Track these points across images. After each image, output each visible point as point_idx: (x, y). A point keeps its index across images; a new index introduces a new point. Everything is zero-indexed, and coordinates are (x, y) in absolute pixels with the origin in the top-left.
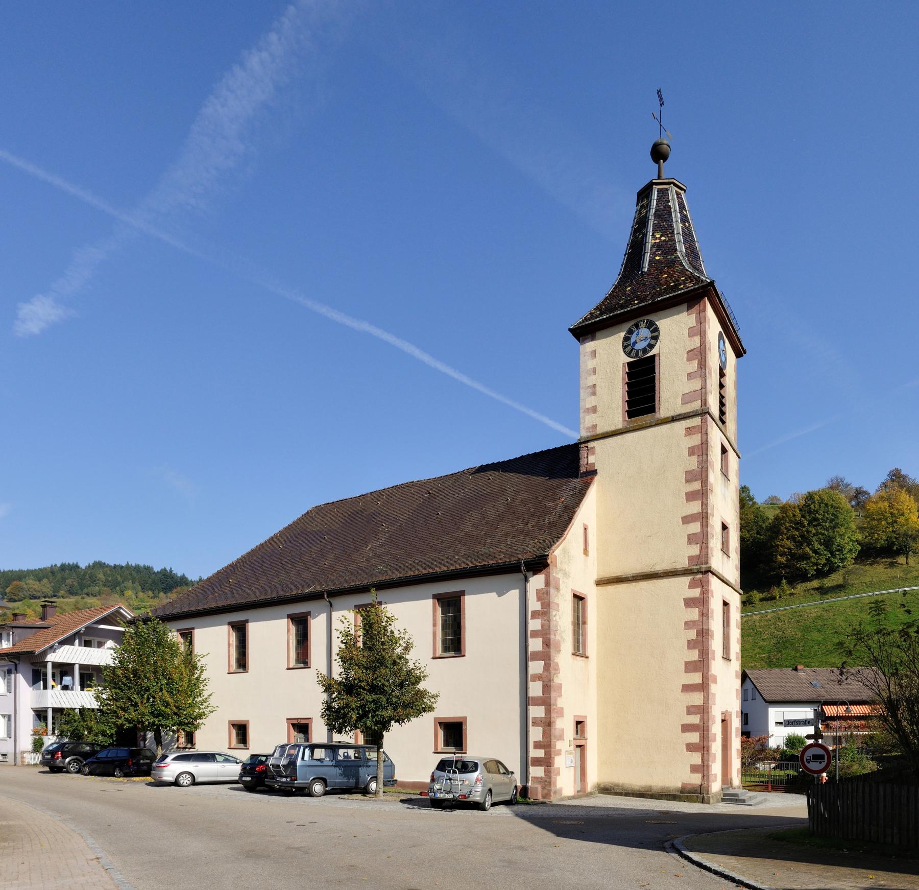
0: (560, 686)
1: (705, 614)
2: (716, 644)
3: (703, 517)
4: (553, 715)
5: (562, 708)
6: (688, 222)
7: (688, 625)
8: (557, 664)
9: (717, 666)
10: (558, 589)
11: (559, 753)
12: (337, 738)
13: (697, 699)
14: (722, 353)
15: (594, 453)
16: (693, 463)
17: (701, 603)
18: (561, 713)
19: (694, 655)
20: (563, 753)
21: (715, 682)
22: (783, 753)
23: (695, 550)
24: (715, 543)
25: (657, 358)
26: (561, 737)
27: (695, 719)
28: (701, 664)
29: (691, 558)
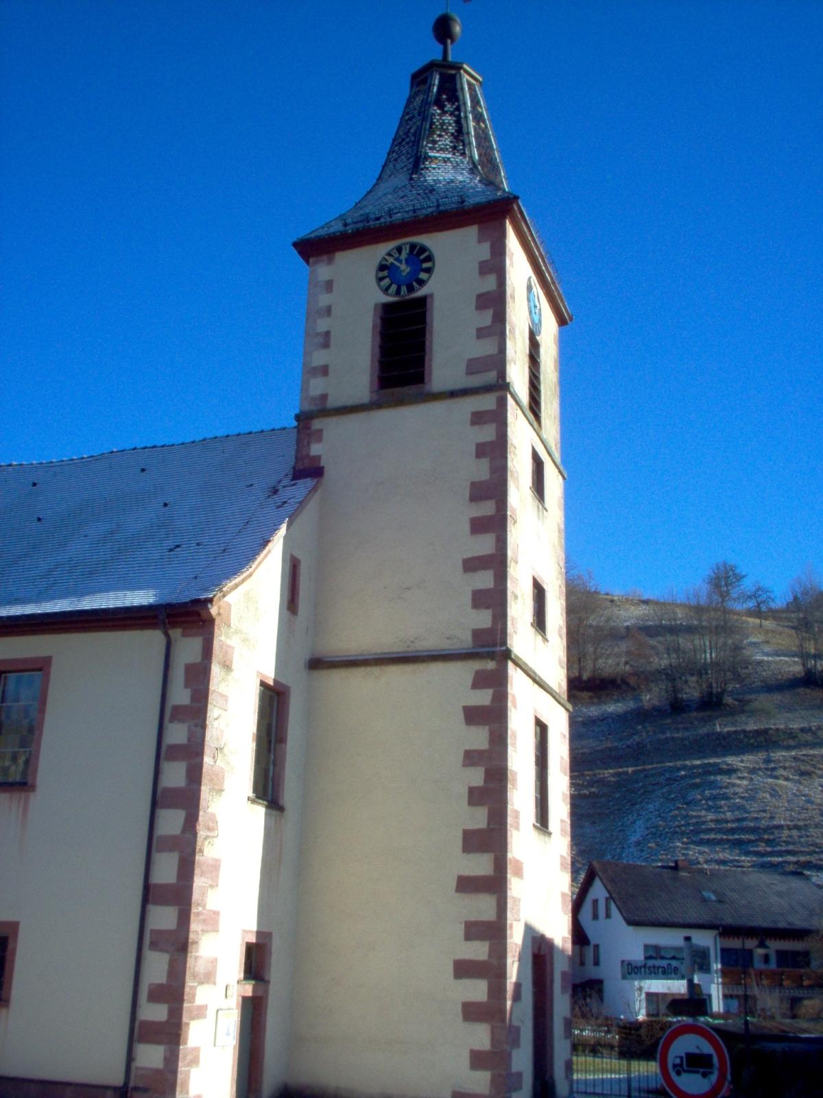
0: (215, 867)
1: (499, 739)
2: (521, 798)
3: (497, 563)
4: (194, 926)
5: (217, 913)
6: (484, 122)
7: (471, 758)
8: (213, 818)
9: (522, 840)
10: (227, 667)
11: (201, 1012)
12: (716, 982)
13: (482, 907)
14: (533, 309)
15: (320, 440)
16: (482, 470)
17: (492, 717)
18: (213, 922)
19: (479, 819)
20: (211, 1013)
21: (519, 873)
22: (492, 1052)
23: (483, 619)
24: (520, 610)
25: (429, 300)
26: (209, 978)
27: (479, 951)
28: (490, 839)
29: (477, 634)
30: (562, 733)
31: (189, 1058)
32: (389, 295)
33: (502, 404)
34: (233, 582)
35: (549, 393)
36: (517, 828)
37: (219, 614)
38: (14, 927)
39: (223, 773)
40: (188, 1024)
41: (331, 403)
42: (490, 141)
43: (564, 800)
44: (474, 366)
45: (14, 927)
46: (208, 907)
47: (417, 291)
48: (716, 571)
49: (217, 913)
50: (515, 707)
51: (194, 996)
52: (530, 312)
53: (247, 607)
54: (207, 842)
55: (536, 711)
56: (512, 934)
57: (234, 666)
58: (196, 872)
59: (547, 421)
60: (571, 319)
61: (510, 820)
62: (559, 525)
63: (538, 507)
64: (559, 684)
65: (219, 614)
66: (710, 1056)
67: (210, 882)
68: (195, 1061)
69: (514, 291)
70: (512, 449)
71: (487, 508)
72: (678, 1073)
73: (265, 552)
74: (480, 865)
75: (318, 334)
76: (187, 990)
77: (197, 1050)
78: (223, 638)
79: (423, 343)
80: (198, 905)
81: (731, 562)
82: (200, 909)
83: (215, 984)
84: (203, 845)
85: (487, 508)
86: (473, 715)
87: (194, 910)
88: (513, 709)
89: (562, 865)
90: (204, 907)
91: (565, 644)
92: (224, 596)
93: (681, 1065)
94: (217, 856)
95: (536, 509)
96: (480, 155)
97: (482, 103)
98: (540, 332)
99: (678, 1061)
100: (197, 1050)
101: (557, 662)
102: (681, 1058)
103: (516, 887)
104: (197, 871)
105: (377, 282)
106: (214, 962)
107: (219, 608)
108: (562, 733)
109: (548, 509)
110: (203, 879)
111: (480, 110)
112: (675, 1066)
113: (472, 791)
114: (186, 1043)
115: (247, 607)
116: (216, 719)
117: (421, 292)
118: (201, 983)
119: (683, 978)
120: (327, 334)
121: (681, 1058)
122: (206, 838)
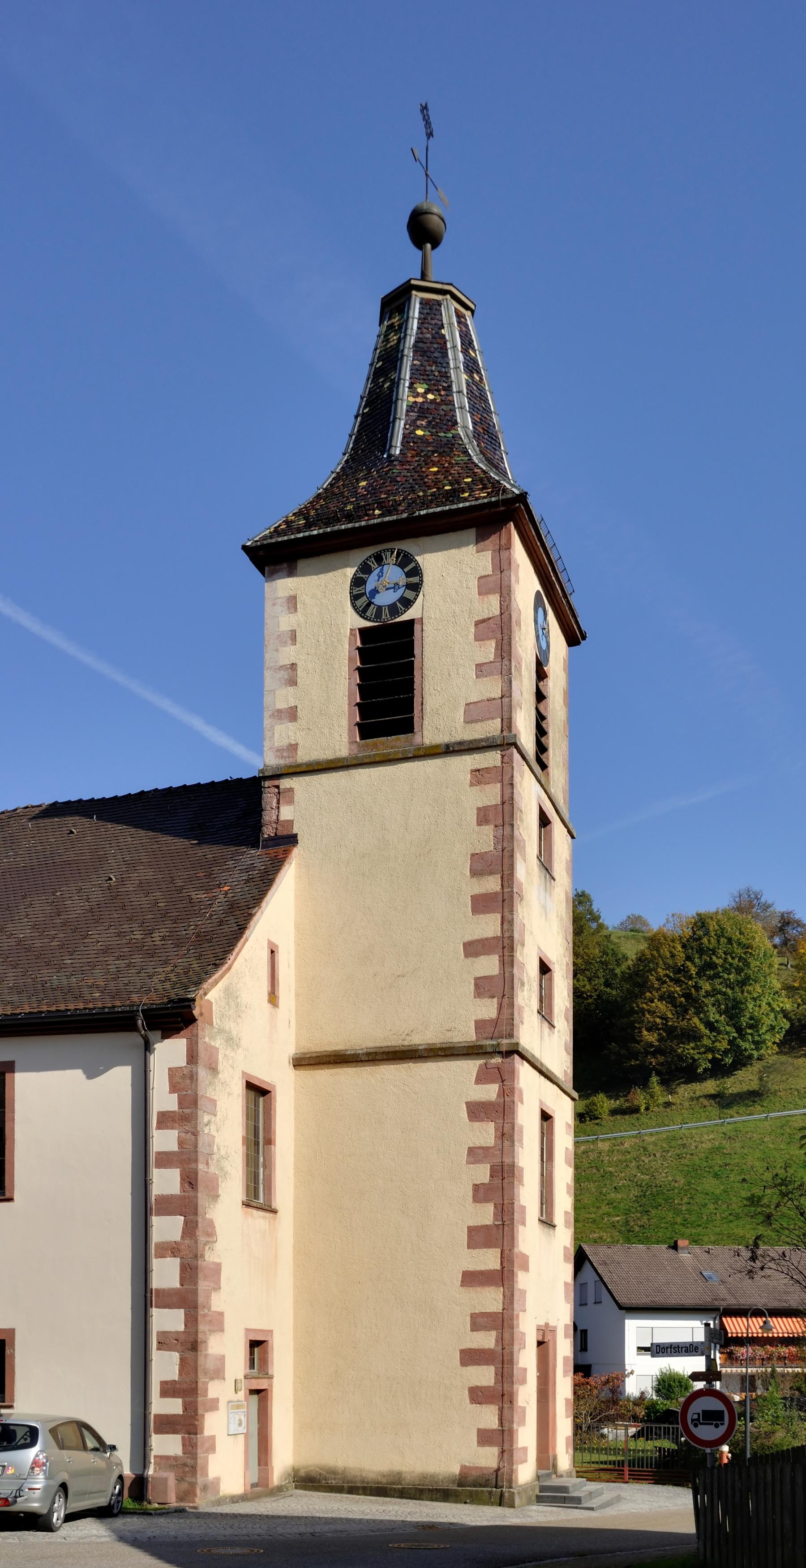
0: (217, 1269)
1: (507, 1135)
2: (528, 1194)
3: (505, 946)
4: (202, 1327)
5: (221, 1314)
6: (479, 373)
8: (211, 1224)
9: (529, 1237)
11: (214, 1405)
13: (490, 1300)
14: (542, 633)
16: (485, 839)
17: (499, 1112)
18: (218, 1323)
20: (222, 1405)
21: (525, 1268)
23: (488, 1009)
24: (527, 998)
25: (417, 627)
28: (499, 1234)
29: (480, 1025)
30: (567, 1123)
31: (207, 1445)
32: (366, 619)
33: (507, 761)
34: (213, 978)
35: (557, 735)
36: (524, 1224)
37: (201, 1014)
38: (12, 1332)
39: (217, 1179)
40: (203, 1416)
41: (304, 756)
42: (486, 401)
43: (568, 1192)
44: (474, 713)
45: (12, 1332)
46: (213, 1309)
47: (402, 614)
48: (737, 899)
49: (221, 1314)
50: (522, 1102)
51: (206, 1390)
52: (537, 637)
53: (228, 1004)
54: (207, 1248)
55: (541, 1102)
56: (518, 1324)
57: (220, 1067)
58: (200, 1276)
59: (556, 772)
60: (584, 638)
61: (516, 1216)
62: (566, 893)
63: (545, 877)
64: (565, 1071)
65: (201, 1014)
66: (723, 1411)
67: (212, 1285)
68: (212, 1449)
69: (520, 615)
70: (519, 814)
71: (492, 884)
72: (696, 1426)
73: (242, 940)
74: (489, 1259)
75: (282, 667)
76: (200, 1385)
77: (213, 1438)
78: (207, 1040)
79: (412, 682)
80: (204, 1307)
81: (756, 888)
82: (206, 1311)
83: (224, 1379)
84: (204, 1250)
85: (492, 884)
86: (477, 1111)
87: (201, 1312)
88: (519, 1104)
89: (565, 1255)
90: (209, 1309)
91: (572, 1027)
92: (205, 994)
93: (698, 1420)
94: (217, 1260)
95: (543, 878)
96: (474, 423)
97: (475, 343)
98: (548, 661)
99: (696, 1417)
100: (213, 1438)
101: (563, 1048)
102: (699, 1414)
103: (523, 1280)
104: (200, 1275)
105: (351, 600)
106: (222, 1358)
107: (201, 1008)
108: (567, 1123)
109: (556, 877)
110: (206, 1283)
111: (473, 355)
112: (693, 1420)
113: (476, 1188)
114: (202, 1433)
115: (228, 1004)
116: (207, 1125)
117: (410, 614)
118: (212, 1379)
119: (702, 1354)
120: (293, 666)
121: (699, 1414)
122: (205, 1244)
